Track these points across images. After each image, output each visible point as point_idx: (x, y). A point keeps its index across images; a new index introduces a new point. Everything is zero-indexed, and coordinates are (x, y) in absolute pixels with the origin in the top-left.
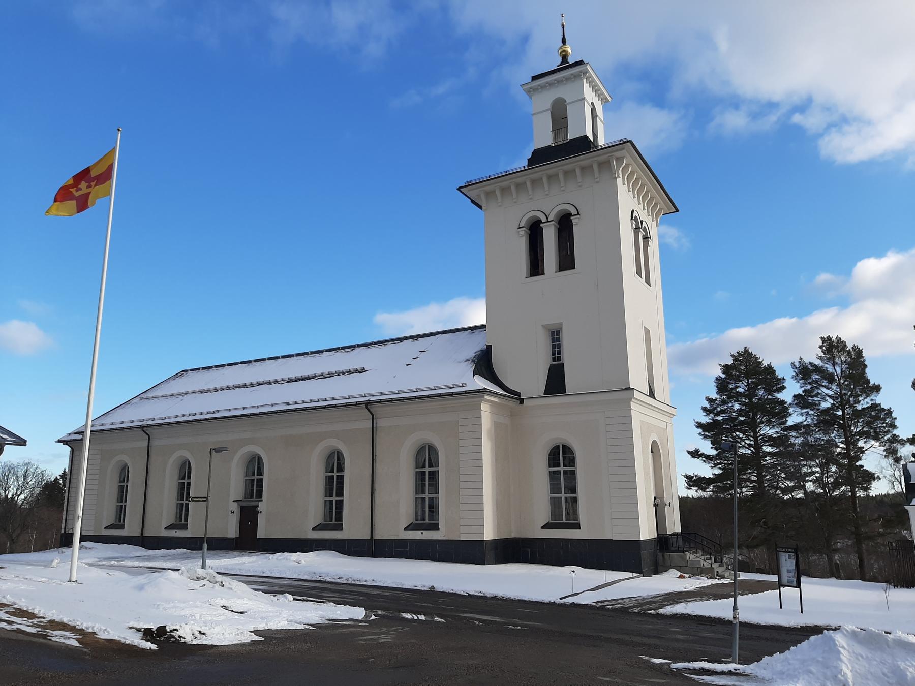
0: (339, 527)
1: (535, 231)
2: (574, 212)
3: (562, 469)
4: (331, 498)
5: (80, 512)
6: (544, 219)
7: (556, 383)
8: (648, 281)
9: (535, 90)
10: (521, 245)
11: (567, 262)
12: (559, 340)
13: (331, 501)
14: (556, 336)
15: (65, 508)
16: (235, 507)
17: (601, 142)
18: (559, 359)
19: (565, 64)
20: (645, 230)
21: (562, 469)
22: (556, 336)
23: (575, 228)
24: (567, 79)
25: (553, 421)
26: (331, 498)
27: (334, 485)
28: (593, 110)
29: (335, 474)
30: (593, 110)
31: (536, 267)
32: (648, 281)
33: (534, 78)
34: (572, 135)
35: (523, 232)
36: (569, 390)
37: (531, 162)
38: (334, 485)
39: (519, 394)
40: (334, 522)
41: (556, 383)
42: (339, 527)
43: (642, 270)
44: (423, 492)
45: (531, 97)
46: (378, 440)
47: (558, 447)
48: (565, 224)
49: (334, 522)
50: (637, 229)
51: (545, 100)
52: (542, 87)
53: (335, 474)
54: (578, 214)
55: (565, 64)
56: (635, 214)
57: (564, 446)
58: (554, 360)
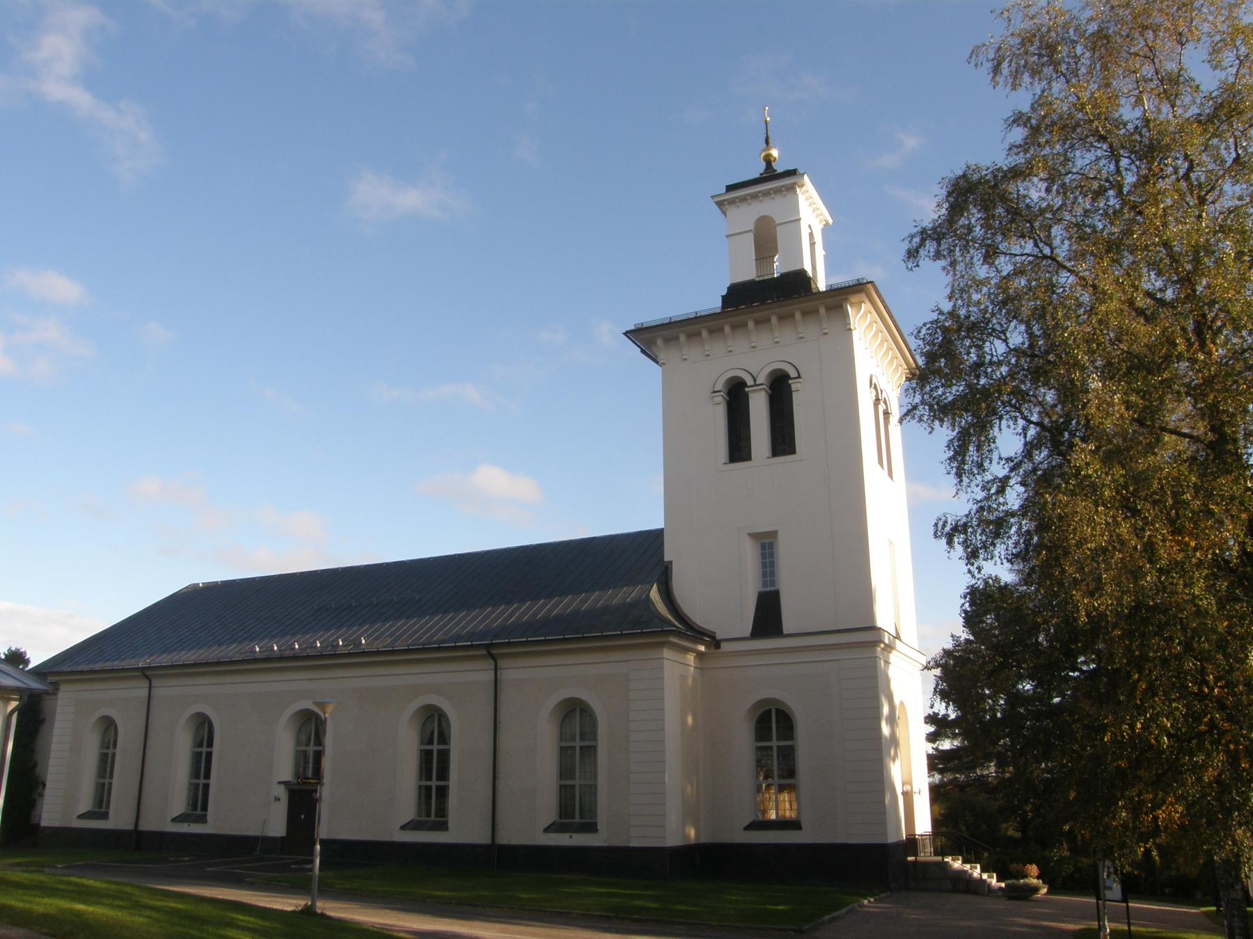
0: (442, 826)
1: (736, 394)
2: (793, 374)
3: (774, 743)
4: (428, 783)
5: (85, 881)
6: (749, 382)
7: (768, 616)
8: (890, 474)
9: (732, 202)
10: (718, 416)
11: (783, 442)
12: (772, 555)
13: (429, 789)
14: (767, 544)
15: (232, 651)
16: (282, 792)
17: (822, 285)
18: (773, 583)
19: (770, 174)
20: (885, 402)
21: (774, 743)
22: (767, 544)
23: (795, 395)
24: (778, 191)
25: (766, 674)
26: (428, 783)
27: (434, 763)
28: (811, 235)
29: (435, 747)
30: (811, 235)
31: (739, 449)
32: (890, 474)
33: (730, 188)
34: (778, 267)
35: (720, 399)
36: (787, 627)
37: (727, 300)
38: (434, 763)
39: (712, 636)
40: (433, 817)
41: (768, 616)
42: (442, 826)
43: (884, 458)
44: (104, 777)
45: (724, 213)
46: (503, 699)
47: (769, 711)
48: (780, 387)
49: (433, 817)
50: (877, 401)
51: (746, 216)
52: (743, 199)
53: (435, 747)
54: (799, 377)
55: (770, 174)
56: (874, 381)
57: (778, 711)
58: (765, 584)
